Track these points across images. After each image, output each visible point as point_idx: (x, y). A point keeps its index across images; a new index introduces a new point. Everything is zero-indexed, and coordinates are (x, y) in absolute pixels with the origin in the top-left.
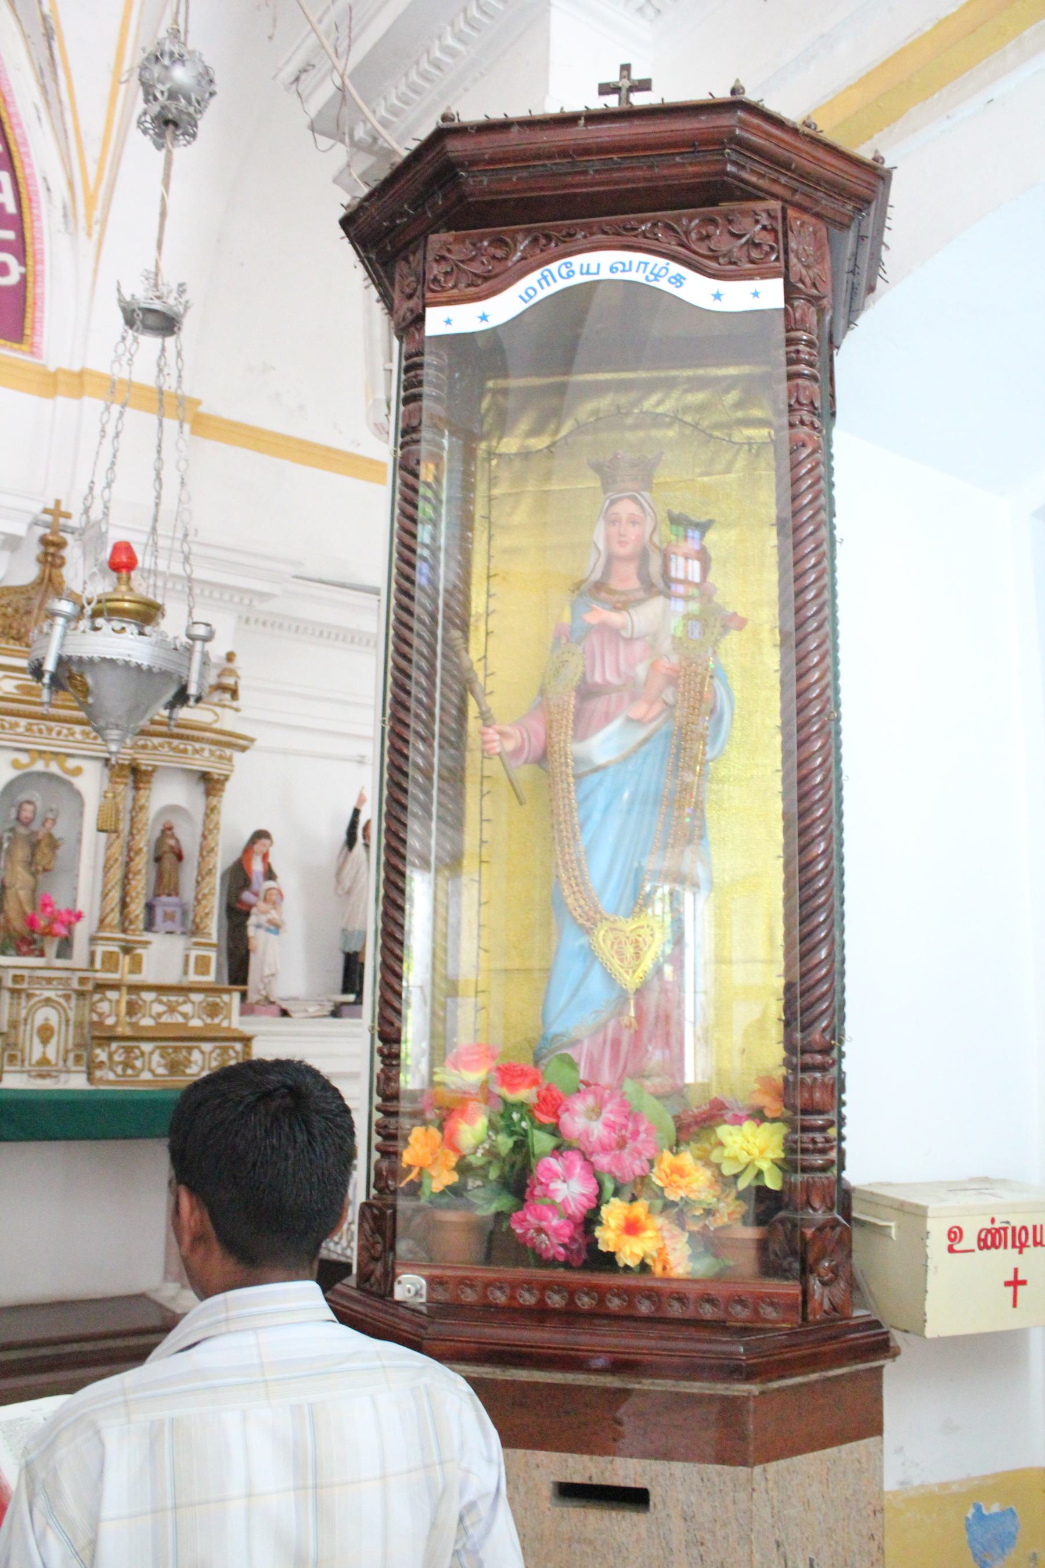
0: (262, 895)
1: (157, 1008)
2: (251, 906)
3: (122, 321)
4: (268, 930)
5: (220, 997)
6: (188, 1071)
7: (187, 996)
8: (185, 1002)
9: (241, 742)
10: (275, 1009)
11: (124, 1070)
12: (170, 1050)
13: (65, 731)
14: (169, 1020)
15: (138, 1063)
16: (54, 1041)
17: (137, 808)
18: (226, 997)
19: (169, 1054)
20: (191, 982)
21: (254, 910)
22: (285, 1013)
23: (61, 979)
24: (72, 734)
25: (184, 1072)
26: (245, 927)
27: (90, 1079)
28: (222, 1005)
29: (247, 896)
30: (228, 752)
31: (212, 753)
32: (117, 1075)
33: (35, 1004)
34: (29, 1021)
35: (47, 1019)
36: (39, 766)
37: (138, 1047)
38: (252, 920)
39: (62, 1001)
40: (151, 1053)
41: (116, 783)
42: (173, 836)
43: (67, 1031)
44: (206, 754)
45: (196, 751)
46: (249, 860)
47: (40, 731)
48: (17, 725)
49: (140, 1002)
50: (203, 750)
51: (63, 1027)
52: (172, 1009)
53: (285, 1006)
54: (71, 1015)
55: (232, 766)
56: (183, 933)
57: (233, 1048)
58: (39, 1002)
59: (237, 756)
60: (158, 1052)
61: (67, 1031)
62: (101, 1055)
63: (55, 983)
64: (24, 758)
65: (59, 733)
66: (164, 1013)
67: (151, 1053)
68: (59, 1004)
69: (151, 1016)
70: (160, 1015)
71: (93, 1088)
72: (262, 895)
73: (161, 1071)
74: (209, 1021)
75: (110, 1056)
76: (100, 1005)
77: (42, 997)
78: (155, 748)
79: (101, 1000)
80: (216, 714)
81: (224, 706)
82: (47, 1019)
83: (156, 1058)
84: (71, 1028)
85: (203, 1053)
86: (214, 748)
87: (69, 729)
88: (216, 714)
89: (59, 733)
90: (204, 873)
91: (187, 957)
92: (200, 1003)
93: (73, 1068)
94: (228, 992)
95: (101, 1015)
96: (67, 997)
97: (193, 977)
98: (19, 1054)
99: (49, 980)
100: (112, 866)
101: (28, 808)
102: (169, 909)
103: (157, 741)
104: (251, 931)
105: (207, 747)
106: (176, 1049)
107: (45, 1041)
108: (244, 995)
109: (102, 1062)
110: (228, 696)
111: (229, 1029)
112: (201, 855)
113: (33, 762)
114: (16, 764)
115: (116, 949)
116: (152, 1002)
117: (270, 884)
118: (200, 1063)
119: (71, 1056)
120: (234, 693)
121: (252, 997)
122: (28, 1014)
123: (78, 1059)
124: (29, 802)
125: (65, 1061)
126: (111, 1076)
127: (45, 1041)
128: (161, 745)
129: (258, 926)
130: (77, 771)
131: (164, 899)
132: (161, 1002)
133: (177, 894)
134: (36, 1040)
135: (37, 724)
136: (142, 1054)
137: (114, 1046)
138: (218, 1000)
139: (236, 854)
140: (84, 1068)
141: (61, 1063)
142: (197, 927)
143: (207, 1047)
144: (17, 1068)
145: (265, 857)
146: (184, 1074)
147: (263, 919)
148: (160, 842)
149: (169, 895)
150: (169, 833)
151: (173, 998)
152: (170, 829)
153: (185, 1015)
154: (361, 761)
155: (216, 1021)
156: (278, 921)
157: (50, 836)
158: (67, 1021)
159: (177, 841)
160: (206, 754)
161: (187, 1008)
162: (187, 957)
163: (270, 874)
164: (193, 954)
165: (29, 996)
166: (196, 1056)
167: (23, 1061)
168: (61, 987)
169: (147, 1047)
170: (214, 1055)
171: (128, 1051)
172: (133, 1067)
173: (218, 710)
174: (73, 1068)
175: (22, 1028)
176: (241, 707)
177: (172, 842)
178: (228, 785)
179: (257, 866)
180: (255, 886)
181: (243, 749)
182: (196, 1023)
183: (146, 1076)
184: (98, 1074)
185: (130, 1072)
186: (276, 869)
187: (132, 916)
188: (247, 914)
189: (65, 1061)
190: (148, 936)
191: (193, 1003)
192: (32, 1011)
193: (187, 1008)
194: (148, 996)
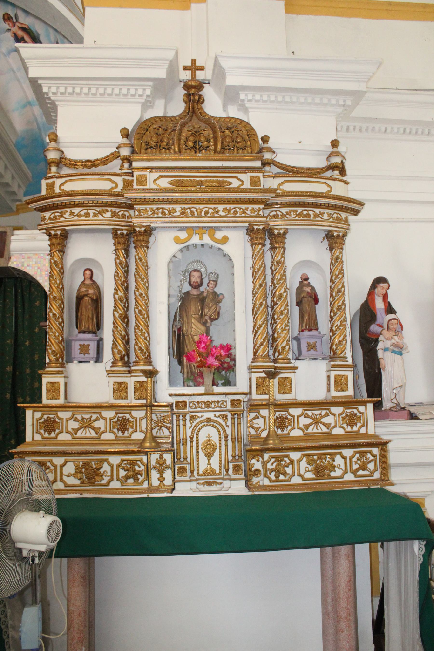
0: (385, 326)
1: (304, 421)
2: (378, 335)
3: (399, 356)
4: (393, 352)
5: (356, 408)
6: (333, 474)
7: (329, 410)
8: (327, 415)
9: (354, 206)
10: (405, 413)
11: (277, 476)
12: (315, 457)
13: (211, 211)
14: (315, 431)
15: (289, 470)
16: (216, 454)
17: (275, 263)
18: (362, 408)
19: (314, 461)
20: (334, 397)
21: (381, 338)
22: (413, 417)
23: (218, 402)
24: (218, 212)
25: (329, 475)
26: (376, 352)
27: (248, 485)
28: (358, 414)
29: (374, 328)
30: (343, 215)
31: (329, 215)
32: (271, 481)
33: (198, 424)
34: (194, 439)
35: (209, 436)
36: (195, 240)
37: (288, 456)
38: (380, 346)
39: (220, 420)
40: (299, 461)
41: (255, 244)
42: (309, 285)
43: (226, 445)
44: (325, 217)
45: (316, 215)
46: (373, 301)
47: (192, 213)
48: (175, 211)
49: (289, 417)
50: (322, 214)
51: (223, 443)
52: (316, 421)
53: (412, 410)
54: (229, 431)
55: (349, 225)
56: (323, 359)
57: (370, 452)
58: (201, 422)
59: (351, 218)
60: (305, 459)
61: (226, 445)
62: (257, 465)
63: (213, 406)
64: (183, 235)
65: (207, 213)
66: (310, 425)
67: (299, 461)
68: (216, 422)
69: (300, 428)
70: (307, 427)
71: (250, 493)
72: (385, 326)
73: (309, 475)
74: (349, 429)
75: (264, 464)
76: (255, 421)
77: (204, 418)
78: (283, 216)
79: (256, 418)
80: (329, 186)
81: (335, 179)
82: (209, 436)
83: (304, 464)
84: (230, 442)
85: (344, 458)
86: (332, 212)
87: (214, 208)
88: (329, 186)
89: (207, 213)
90: (335, 309)
91: (329, 377)
92: (111, 419)
93: (233, 477)
94: (364, 403)
95: (257, 429)
96: (225, 417)
97: (334, 393)
98: (188, 466)
99: (208, 404)
100: (258, 309)
101: (196, 274)
102: (311, 341)
103: (284, 210)
104: (380, 354)
105: (325, 211)
106: (320, 456)
107: (209, 455)
108: (378, 406)
109: (258, 470)
110: (337, 172)
111: (366, 435)
112: (332, 296)
113: (189, 238)
114: (177, 240)
115: (263, 375)
116: (300, 416)
117: (392, 316)
118: (343, 467)
119: (231, 466)
120: (342, 171)
121: (387, 405)
122: (192, 433)
123: (237, 468)
124: (195, 271)
125: (227, 471)
126: (266, 482)
127: (209, 455)
128: (289, 213)
129: (386, 350)
130: (225, 240)
131: (306, 333)
132: (307, 416)
133: (317, 329)
134: (202, 454)
135: (189, 208)
136: (292, 462)
137: (266, 456)
138: (355, 411)
139: (363, 298)
140: (242, 476)
141: (224, 472)
142: (335, 353)
143: (348, 453)
144: (187, 478)
145: (385, 297)
146: (329, 477)
147: (388, 344)
148: (299, 290)
149: (310, 330)
150: (305, 282)
151: (87, 416)
152: (307, 279)
153: (327, 425)
154: (400, 543)
155: (355, 429)
156: (400, 344)
157: (215, 293)
158: (226, 437)
159: (313, 288)
160: (325, 217)
161: (330, 420)
162: (329, 377)
163: (390, 310)
164: (333, 374)
165: (192, 418)
166: (338, 460)
167: (192, 472)
168: (218, 409)
169: (295, 456)
170: (355, 459)
171: (279, 459)
172: (285, 474)
173: (329, 182)
174: (233, 477)
175: (189, 444)
176: (348, 180)
177: (308, 289)
178: (348, 240)
179: (379, 305)
180: (379, 320)
181: (356, 212)
182: (278, 446)
183: (296, 480)
184: (255, 480)
185: (282, 477)
186: (394, 306)
187: (280, 348)
188: (377, 341)
189: (227, 471)
190: (297, 363)
191: (334, 415)
192: (196, 430)
193: (330, 420)
194: (296, 412)
